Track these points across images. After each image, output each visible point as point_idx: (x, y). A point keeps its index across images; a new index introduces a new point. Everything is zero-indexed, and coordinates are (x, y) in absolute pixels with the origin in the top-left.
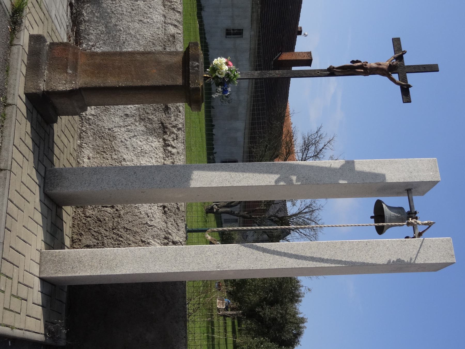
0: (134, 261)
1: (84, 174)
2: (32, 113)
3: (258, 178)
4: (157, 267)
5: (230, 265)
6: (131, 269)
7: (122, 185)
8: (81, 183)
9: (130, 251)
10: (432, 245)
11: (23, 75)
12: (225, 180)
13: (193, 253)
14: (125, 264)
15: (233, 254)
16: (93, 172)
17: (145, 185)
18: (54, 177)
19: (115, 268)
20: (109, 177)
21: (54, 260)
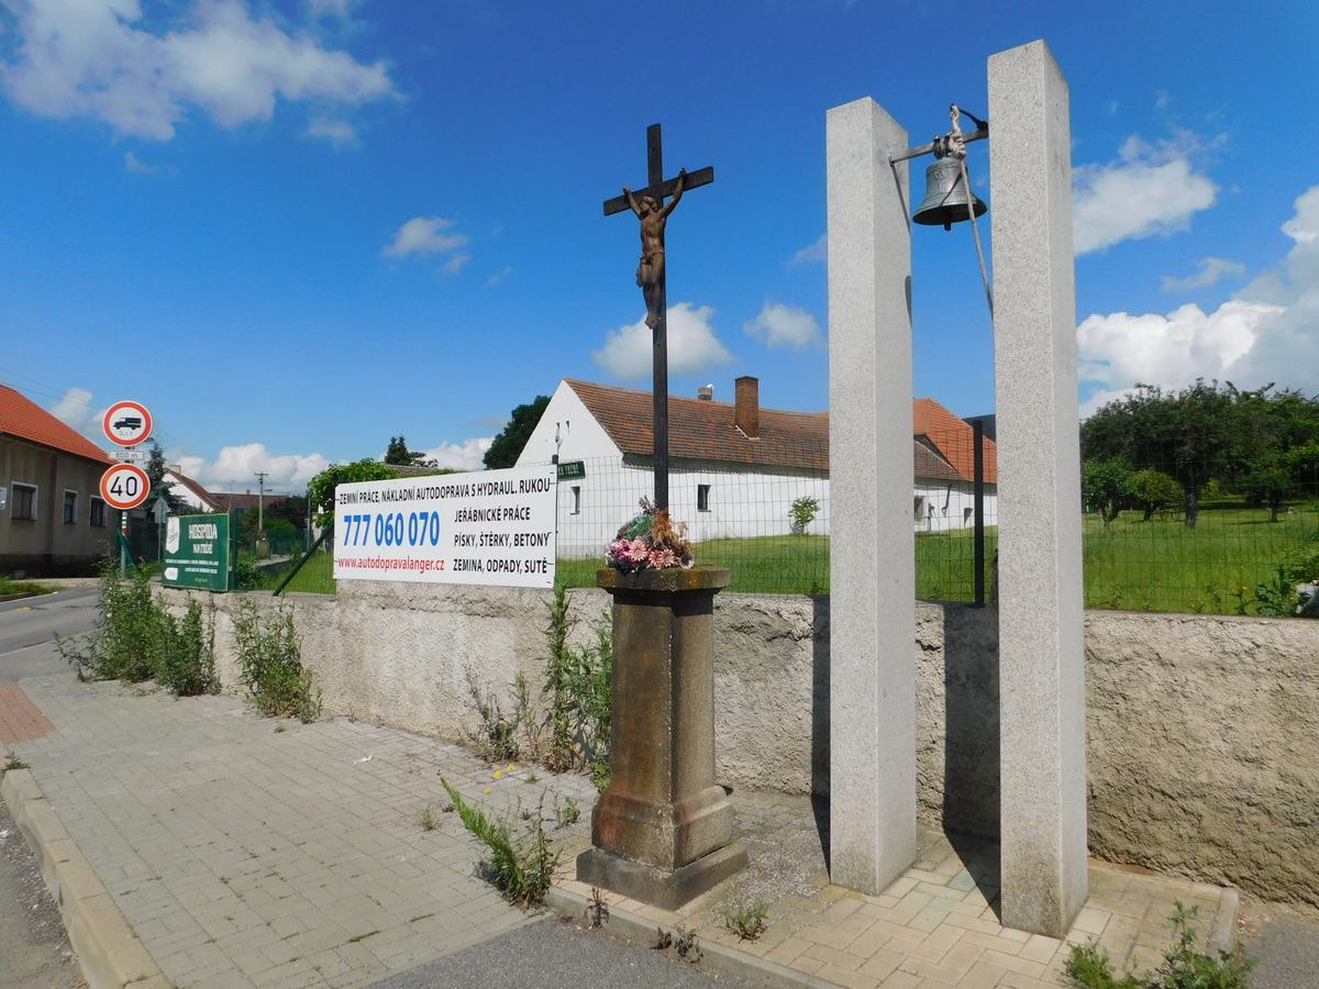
6: (1048, 737)
10: (1004, 95)
21: (1024, 901)
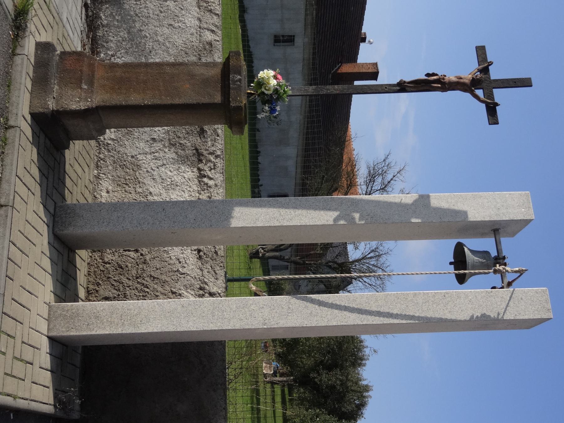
0: (162, 317)
1: (102, 211)
2: (39, 137)
3: (312, 216)
4: (191, 323)
5: (279, 322)
6: (159, 326)
7: (148, 224)
8: (98, 222)
9: (158, 304)
10: (523, 298)
11: (28, 91)
12: (273, 218)
13: (234, 307)
14: (151, 320)
15: (283, 308)
16: (113, 209)
17: (176, 224)
18: (66, 214)
19: (139, 325)
20: (132, 214)
21: (65, 316)
